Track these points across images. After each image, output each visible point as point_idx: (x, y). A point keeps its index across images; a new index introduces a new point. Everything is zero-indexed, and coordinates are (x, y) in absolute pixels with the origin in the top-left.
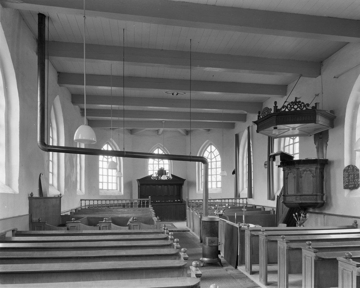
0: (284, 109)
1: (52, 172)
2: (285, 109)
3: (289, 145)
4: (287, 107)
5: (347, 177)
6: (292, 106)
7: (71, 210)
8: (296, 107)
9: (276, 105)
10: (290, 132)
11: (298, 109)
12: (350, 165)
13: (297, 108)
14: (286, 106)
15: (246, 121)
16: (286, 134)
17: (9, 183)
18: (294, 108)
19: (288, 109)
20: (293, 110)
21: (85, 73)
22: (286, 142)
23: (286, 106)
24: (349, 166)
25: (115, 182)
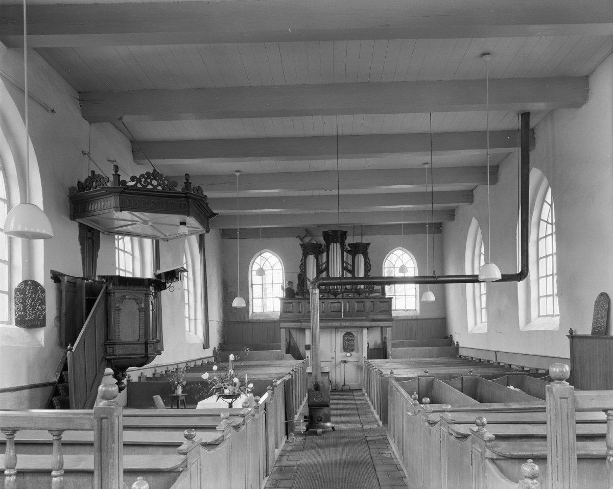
0: (134, 183)
1: (188, 316)
2: (136, 184)
3: (546, 236)
4: (139, 181)
5: (21, 303)
6: (149, 180)
7: (372, 327)
8: (155, 183)
9: (116, 172)
10: (138, 228)
11: (160, 188)
12: (28, 281)
13: (157, 186)
14: (138, 177)
15: (455, 219)
16: (130, 228)
17: (206, 346)
18: (152, 185)
19: (141, 184)
20: (150, 187)
21: (490, 164)
22: (540, 232)
23: (138, 177)
24: (25, 283)
25: (399, 287)
